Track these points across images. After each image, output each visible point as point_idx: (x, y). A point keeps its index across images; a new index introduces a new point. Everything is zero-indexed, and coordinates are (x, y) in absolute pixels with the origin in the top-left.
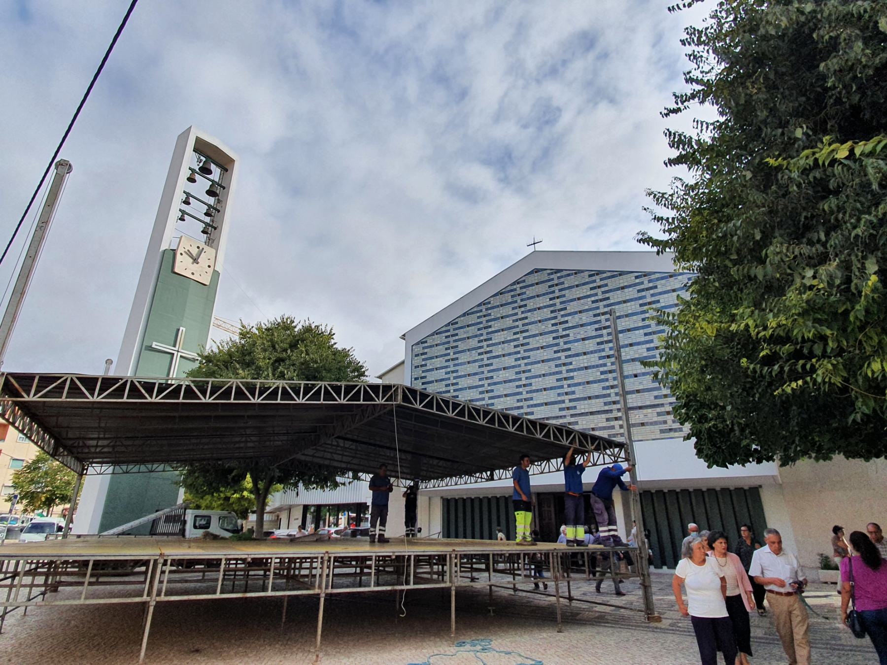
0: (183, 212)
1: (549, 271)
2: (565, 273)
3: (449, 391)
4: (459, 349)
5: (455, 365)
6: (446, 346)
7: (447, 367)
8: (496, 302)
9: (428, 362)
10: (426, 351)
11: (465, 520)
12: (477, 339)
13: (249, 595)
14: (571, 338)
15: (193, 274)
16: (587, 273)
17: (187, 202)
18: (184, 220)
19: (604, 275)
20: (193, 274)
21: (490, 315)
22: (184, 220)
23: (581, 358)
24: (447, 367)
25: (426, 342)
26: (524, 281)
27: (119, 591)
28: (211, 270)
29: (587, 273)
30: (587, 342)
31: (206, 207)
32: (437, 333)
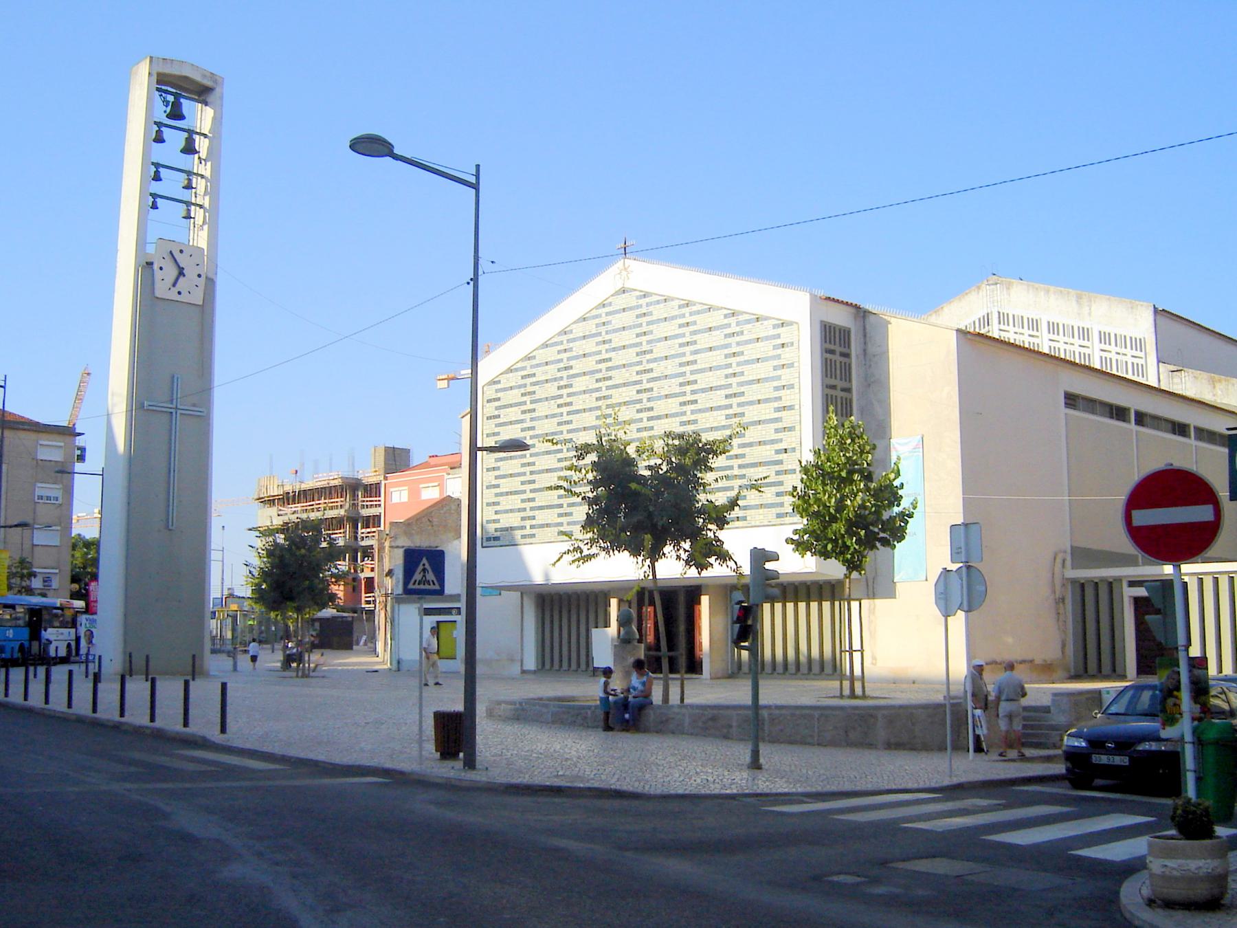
0: (154, 196)
1: (638, 293)
2: (655, 298)
3: (562, 432)
4: (537, 397)
5: (532, 419)
6: (523, 390)
7: (522, 421)
8: (579, 330)
9: (502, 412)
10: (499, 395)
11: (552, 628)
12: (556, 384)
13: (948, 722)
14: (655, 394)
15: (181, 251)
16: (676, 303)
17: (157, 178)
18: (162, 141)
19: (694, 308)
20: (181, 251)
21: (571, 350)
22: (162, 141)
23: (663, 421)
24: (522, 421)
25: (499, 382)
26: (610, 304)
27: (989, 805)
28: (202, 280)
29: (676, 303)
30: (670, 400)
31: (184, 176)
32: (510, 370)
